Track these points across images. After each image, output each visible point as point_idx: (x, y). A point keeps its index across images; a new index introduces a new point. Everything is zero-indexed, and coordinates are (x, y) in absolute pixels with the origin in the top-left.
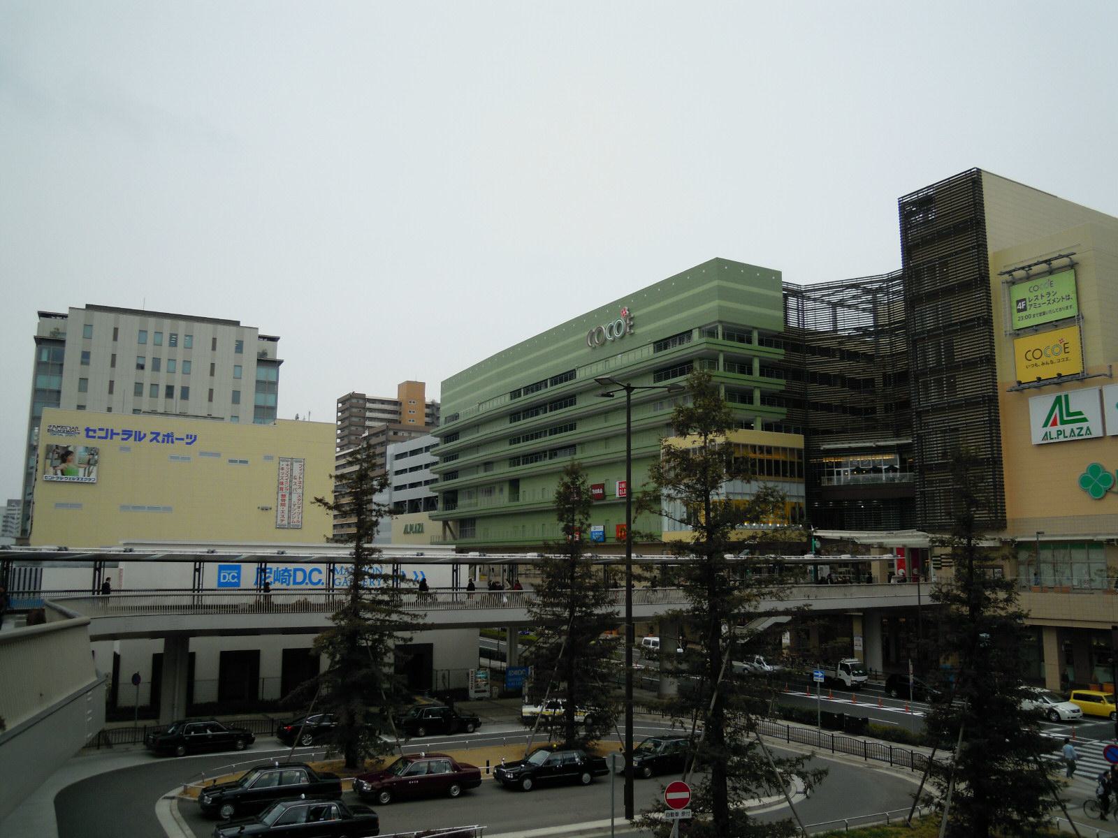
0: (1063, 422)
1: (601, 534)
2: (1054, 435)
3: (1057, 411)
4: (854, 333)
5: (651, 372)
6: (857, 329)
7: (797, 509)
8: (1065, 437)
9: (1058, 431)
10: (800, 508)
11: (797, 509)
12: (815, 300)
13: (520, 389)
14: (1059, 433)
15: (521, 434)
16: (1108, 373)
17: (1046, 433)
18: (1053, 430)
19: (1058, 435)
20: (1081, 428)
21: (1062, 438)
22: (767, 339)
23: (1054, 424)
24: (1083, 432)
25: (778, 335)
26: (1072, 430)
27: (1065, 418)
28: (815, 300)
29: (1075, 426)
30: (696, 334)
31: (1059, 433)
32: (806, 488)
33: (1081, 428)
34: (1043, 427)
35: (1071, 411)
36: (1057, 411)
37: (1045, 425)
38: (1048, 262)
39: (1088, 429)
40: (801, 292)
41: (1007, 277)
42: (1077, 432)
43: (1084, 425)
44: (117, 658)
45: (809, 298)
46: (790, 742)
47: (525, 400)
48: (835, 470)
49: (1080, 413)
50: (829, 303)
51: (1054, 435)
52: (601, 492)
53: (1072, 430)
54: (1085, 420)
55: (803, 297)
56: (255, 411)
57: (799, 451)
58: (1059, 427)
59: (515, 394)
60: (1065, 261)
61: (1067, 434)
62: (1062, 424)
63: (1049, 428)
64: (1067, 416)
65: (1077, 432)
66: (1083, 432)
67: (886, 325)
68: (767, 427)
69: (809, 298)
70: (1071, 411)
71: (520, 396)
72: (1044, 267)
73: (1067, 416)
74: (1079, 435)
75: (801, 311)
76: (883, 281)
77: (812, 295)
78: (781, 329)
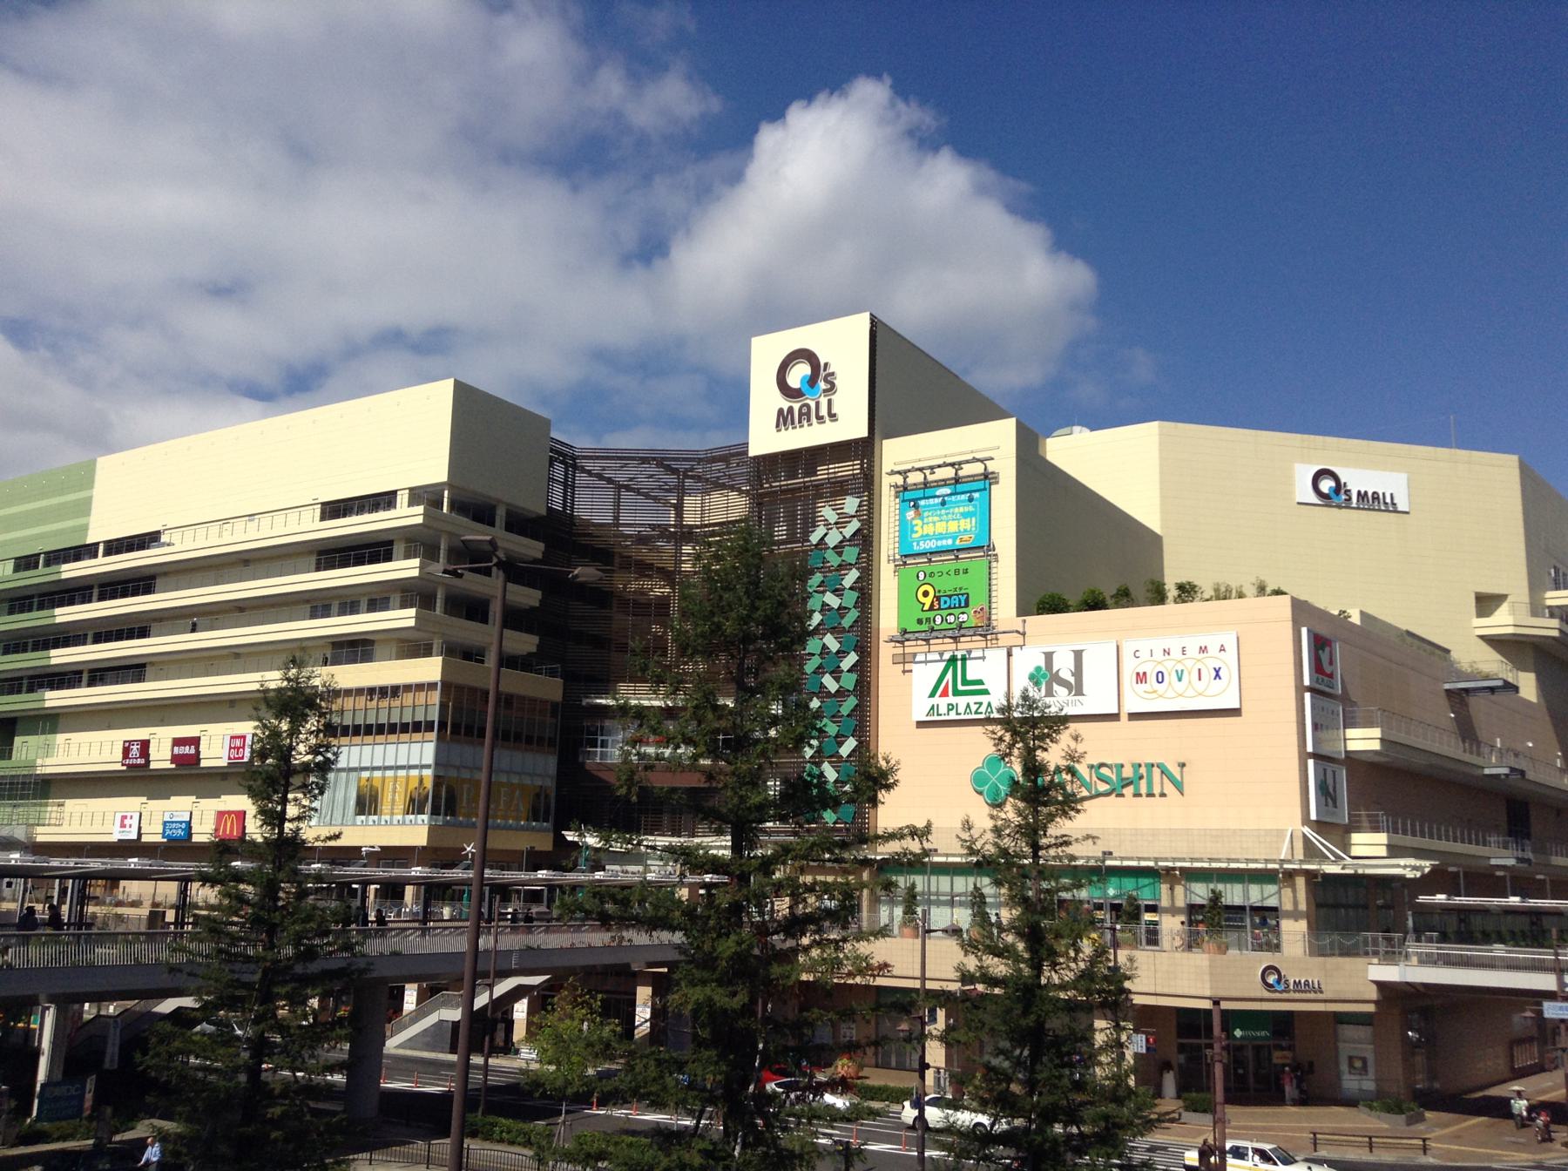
0: (957, 693)
1: (183, 826)
2: (943, 710)
3: (949, 676)
4: (646, 531)
5: (310, 553)
6: (653, 527)
7: (542, 798)
8: (957, 714)
9: (949, 705)
10: (547, 796)
11: (542, 798)
12: (589, 473)
13: (39, 554)
14: (951, 707)
15: (32, 637)
16: (1021, 630)
17: (933, 707)
18: (943, 703)
19: (949, 710)
20: (981, 704)
21: (953, 716)
22: (519, 523)
23: (945, 694)
24: (983, 709)
25: (538, 520)
26: (968, 706)
27: (960, 687)
28: (589, 473)
29: (972, 699)
30: (403, 498)
31: (951, 707)
32: (560, 763)
33: (981, 704)
34: (989, 694)
35: (969, 677)
36: (949, 676)
37: (932, 695)
38: (956, 465)
39: (989, 705)
40: (574, 458)
41: (899, 480)
42: (974, 708)
43: (984, 699)
44: (1315, 1151)
45: (583, 470)
46: (430, 1166)
47: (39, 576)
48: (600, 738)
49: (980, 682)
50: (610, 480)
51: (943, 710)
52: (193, 751)
53: (968, 706)
54: (986, 692)
55: (575, 467)
56: (121, 450)
57: (555, 705)
58: (952, 699)
59: (26, 563)
60: (977, 468)
61: (961, 710)
62: (954, 695)
63: (937, 700)
64: (963, 685)
65: (974, 708)
66: (983, 709)
67: (697, 527)
68: (508, 661)
69: (583, 470)
70: (969, 677)
71: (96, 556)
72: (949, 473)
73: (963, 685)
74: (976, 713)
75: (569, 486)
76: (700, 460)
77: (589, 465)
78: (543, 512)
